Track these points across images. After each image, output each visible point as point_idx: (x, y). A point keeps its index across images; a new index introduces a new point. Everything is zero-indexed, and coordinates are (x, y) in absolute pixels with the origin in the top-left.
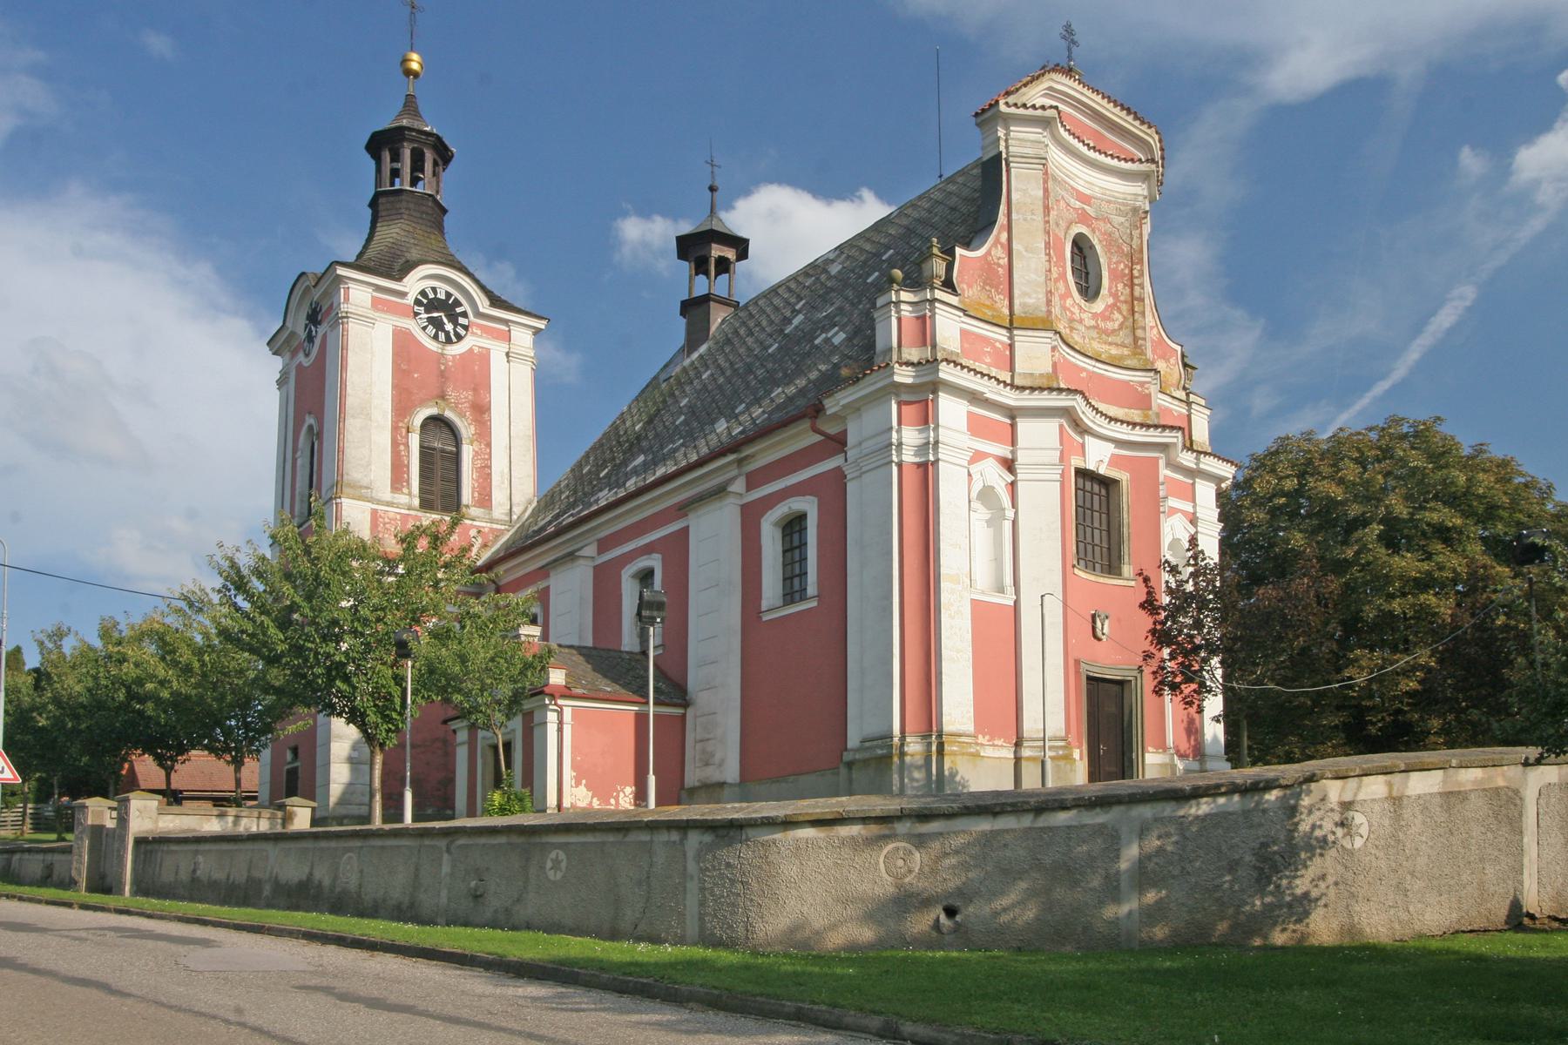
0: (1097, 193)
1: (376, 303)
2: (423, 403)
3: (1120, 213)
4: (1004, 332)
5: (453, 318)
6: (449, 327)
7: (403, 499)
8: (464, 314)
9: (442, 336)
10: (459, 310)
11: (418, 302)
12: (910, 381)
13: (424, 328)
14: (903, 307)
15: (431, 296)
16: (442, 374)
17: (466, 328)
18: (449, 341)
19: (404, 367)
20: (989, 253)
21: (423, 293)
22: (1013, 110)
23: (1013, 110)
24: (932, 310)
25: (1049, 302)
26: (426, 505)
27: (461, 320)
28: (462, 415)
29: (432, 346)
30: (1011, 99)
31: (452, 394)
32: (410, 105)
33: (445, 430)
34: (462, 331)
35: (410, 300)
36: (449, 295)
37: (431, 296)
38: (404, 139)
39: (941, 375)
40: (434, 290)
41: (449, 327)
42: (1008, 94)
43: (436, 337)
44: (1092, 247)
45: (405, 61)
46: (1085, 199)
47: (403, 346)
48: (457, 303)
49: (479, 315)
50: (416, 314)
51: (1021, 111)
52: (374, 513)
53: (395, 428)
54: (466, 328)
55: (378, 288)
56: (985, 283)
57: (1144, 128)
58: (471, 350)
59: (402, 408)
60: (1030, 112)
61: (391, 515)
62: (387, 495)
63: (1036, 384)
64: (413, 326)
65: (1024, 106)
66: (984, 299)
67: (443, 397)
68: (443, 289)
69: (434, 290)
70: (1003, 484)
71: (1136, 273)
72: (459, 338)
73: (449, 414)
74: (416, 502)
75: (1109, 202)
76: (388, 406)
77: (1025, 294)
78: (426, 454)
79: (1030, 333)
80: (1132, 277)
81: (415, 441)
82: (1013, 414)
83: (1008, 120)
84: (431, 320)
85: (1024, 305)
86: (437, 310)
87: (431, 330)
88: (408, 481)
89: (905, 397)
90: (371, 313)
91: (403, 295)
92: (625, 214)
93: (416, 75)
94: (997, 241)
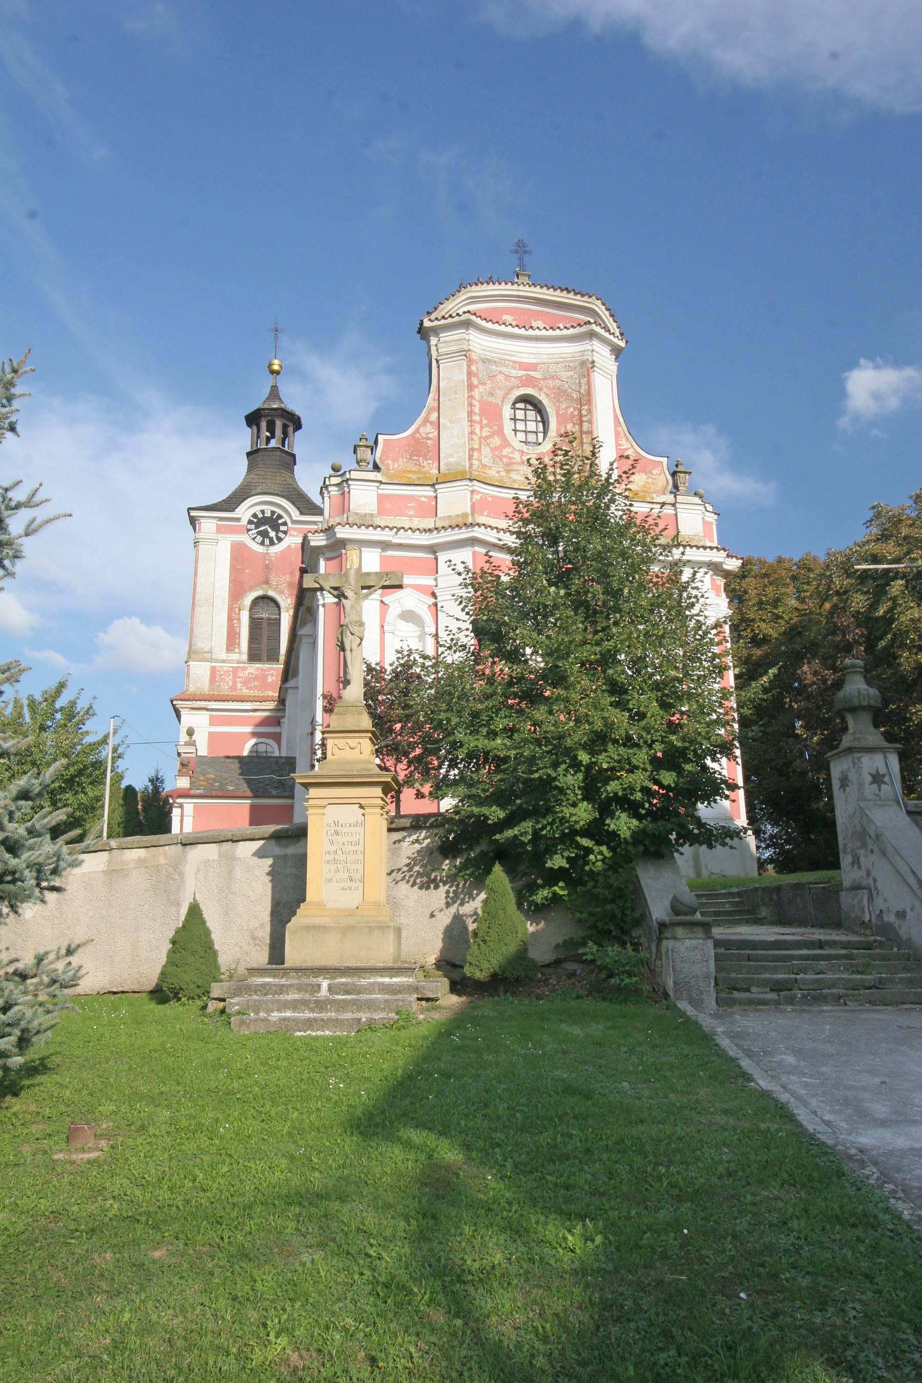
0: (544, 358)
1: (219, 530)
2: (252, 588)
3: (568, 368)
4: (429, 488)
5: (276, 528)
6: (272, 534)
7: (234, 656)
8: (285, 524)
9: (267, 541)
10: (280, 521)
11: (250, 522)
12: (324, 543)
13: (254, 539)
14: (330, 488)
15: (260, 516)
16: (267, 567)
17: (285, 533)
18: (272, 543)
19: (238, 567)
20: (417, 431)
21: (255, 516)
22: (436, 323)
23: (436, 323)
24: (349, 486)
25: (471, 457)
26: (254, 656)
27: (282, 528)
28: (281, 592)
29: (260, 549)
30: (433, 317)
31: (274, 579)
32: (274, 393)
33: (272, 604)
34: (281, 535)
35: (244, 521)
36: (273, 513)
37: (260, 516)
38: (260, 418)
39: (339, 535)
40: (263, 512)
41: (272, 534)
42: (429, 313)
43: (262, 543)
44: (540, 401)
45: (270, 365)
46: (523, 366)
47: (239, 554)
48: (280, 517)
49: (294, 522)
50: (248, 530)
51: (443, 322)
52: (213, 670)
53: (231, 609)
54: (285, 533)
55: (221, 519)
56: (412, 455)
57: (586, 298)
58: (289, 547)
59: (236, 594)
60: (450, 320)
61: (225, 669)
62: (223, 655)
63: (454, 523)
64: (246, 539)
65: (458, 315)
66: (410, 466)
67: (267, 582)
68: (268, 510)
69: (263, 512)
70: (425, 607)
71: (584, 412)
72: (280, 540)
73: (271, 593)
74: (245, 657)
75: (558, 363)
76: (226, 594)
77: (449, 456)
78: (255, 624)
79: (448, 485)
80: (581, 416)
81: (245, 616)
82: (433, 549)
83: (436, 331)
84: (259, 533)
85: (448, 464)
86: (264, 524)
87: (259, 539)
88: (239, 644)
89: (328, 555)
90: (215, 536)
91: (238, 519)
92: (853, 365)
93: (278, 373)
94: (426, 420)
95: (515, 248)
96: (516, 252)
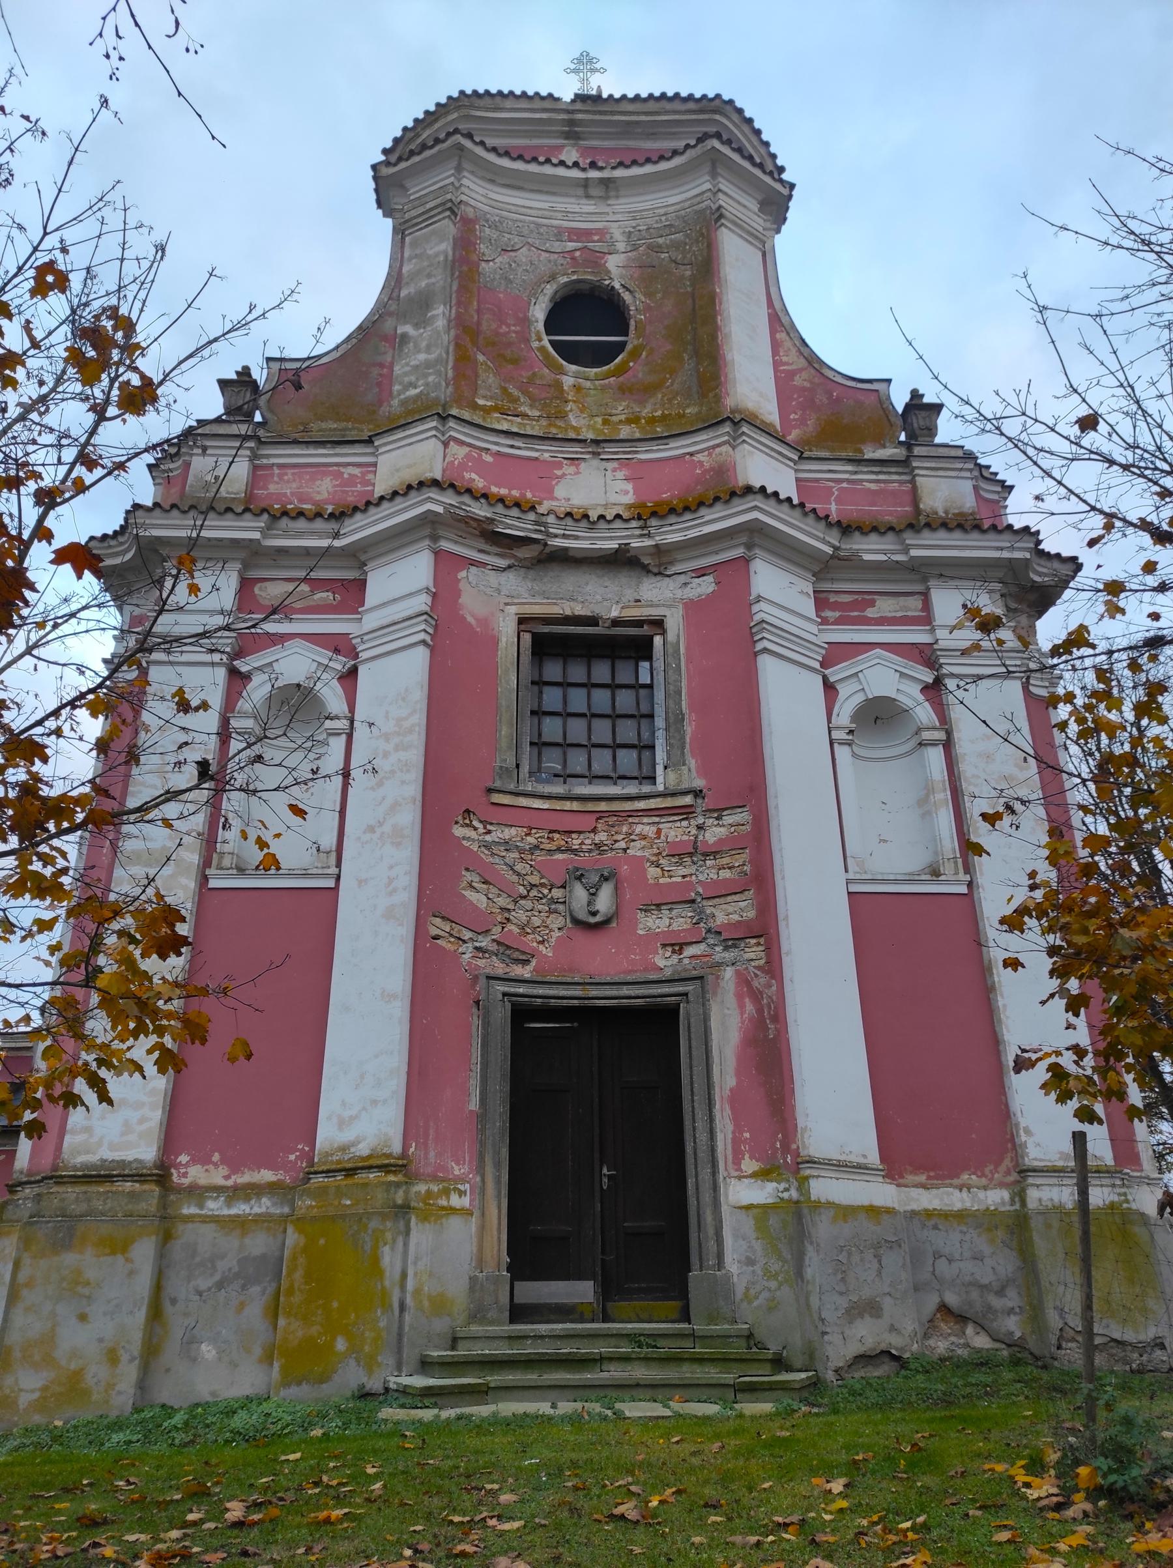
95: (573, 66)
96: (576, 71)
